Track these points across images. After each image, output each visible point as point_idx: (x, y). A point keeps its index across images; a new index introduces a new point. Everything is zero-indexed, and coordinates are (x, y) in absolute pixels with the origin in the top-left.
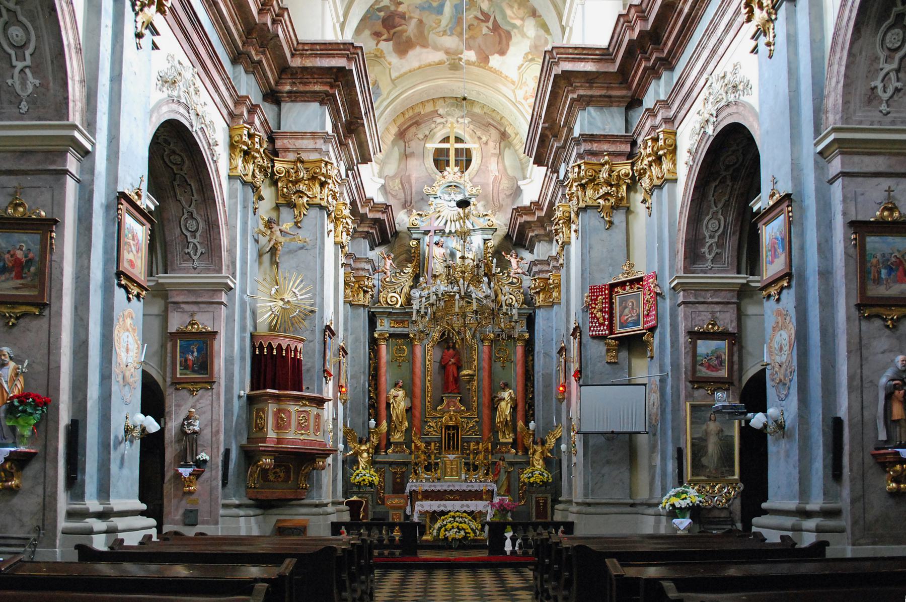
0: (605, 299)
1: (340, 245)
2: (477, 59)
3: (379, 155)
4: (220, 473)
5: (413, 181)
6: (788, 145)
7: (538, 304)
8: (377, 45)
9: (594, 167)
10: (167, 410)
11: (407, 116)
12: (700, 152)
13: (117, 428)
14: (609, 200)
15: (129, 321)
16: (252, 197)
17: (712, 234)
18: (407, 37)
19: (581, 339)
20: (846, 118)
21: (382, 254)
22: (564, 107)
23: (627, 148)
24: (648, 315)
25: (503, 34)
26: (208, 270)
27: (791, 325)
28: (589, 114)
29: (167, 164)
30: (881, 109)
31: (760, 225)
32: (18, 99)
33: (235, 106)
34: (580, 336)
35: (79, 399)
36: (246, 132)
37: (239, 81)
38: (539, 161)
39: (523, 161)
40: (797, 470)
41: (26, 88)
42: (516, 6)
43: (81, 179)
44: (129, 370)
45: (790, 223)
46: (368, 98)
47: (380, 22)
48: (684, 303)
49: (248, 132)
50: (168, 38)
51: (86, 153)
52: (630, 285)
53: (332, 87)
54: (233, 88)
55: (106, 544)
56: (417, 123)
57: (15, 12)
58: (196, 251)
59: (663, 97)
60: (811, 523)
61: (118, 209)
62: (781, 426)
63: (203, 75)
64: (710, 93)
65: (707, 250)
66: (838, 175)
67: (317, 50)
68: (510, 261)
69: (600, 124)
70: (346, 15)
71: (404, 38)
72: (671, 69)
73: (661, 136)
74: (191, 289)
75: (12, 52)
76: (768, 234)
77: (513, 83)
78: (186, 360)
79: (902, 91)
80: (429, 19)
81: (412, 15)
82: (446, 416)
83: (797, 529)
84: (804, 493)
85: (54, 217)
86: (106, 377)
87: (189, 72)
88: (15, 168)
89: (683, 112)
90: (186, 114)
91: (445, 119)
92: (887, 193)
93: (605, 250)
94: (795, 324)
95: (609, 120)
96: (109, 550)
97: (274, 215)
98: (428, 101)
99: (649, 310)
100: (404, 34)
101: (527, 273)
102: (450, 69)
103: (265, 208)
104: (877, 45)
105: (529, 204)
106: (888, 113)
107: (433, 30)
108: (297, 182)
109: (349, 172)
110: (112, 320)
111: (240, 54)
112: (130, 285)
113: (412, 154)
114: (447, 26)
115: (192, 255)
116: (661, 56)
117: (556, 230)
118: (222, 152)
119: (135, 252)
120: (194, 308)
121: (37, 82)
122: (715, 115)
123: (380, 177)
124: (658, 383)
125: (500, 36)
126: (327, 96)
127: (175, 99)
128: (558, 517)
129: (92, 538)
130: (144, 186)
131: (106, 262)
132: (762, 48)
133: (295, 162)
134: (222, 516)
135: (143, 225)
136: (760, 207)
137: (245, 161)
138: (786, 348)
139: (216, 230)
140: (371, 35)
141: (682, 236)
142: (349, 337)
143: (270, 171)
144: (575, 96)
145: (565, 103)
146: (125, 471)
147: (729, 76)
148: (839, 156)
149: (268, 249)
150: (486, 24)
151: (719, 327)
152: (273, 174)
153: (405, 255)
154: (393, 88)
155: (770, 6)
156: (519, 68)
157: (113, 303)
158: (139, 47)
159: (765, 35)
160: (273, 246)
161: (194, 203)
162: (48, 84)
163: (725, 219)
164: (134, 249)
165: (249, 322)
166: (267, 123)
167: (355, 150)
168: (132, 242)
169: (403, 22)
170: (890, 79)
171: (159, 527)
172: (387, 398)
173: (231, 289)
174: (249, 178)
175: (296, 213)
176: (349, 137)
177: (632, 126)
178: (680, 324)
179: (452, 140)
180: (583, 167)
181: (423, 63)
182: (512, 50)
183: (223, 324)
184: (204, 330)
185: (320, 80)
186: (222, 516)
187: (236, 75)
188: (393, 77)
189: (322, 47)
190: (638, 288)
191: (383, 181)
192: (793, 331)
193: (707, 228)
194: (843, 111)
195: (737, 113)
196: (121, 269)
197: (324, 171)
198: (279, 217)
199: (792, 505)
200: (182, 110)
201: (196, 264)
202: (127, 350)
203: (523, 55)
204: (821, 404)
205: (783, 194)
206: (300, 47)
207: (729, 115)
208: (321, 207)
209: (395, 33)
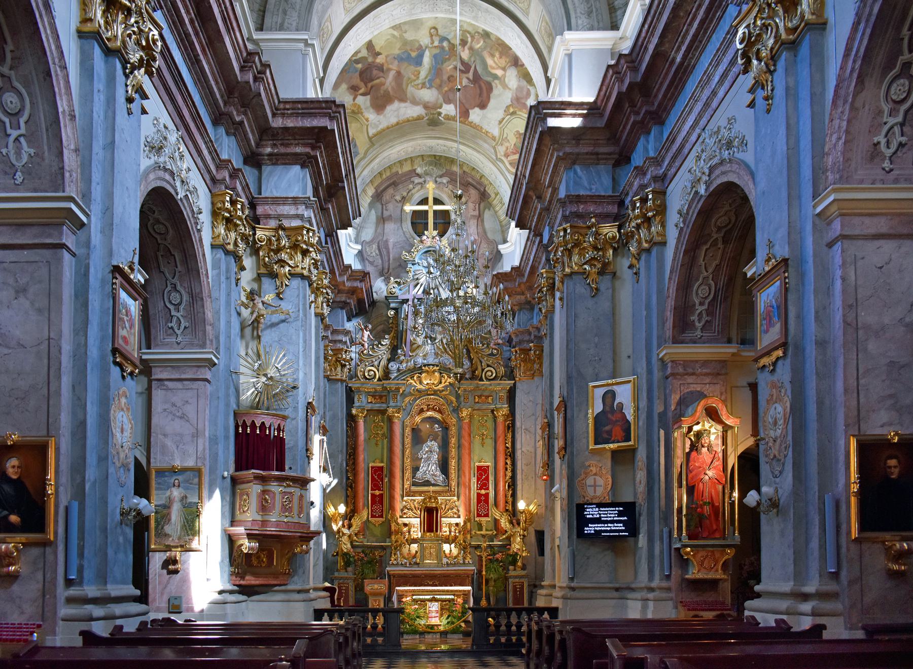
1: (320, 316)
3: (358, 220)
5: (391, 246)
8: (354, 99)
11: (384, 176)
12: (691, 213)
14: (595, 266)
15: (123, 400)
16: (235, 269)
17: (702, 300)
18: (385, 91)
22: (549, 166)
23: (613, 209)
25: (483, 85)
26: (192, 345)
27: (786, 398)
28: (575, 172)
29: (151, 235)
30: (884, 166)
31: (754, 292)
32: (11, 171)
35: (78, 481)
36: (228, 199)
37: (221, 144)
38: (521, 225)
39: (504, 223)
40: (792, 550)
41: (21, 158)
42: (497, 55)
44: (124, 451)
45: (786, 290)
46: (349, 159)
47: (357, 74)
49: (231, 198)
50: (155, 104)
53: (314, 148)
54: (216, 151)
56: (394, 184)
57: (9, 78)
58: (180, 326)
60: (807, 607)
61: (113, 284)
63: (187, 138)
65: (697, 318)
66: (837, 238)
67: (299, 109)
69: (586, 184)
71: (382, 92)
72: (662, 123)
73: (650, 197)
75: (7, 120)
76: (762, 302)
77: (494, 138)
79: (907, 146)
80: (408, 71)
81: (391, 66)
86: (103, 459)
88: (11, 242)
89: (673, 170)
90: (172, 181)
91: (423, 179)
93: (590, 319)
94: (790, 397)
96: (109, 636)
97: (255, 286)
98: (406, 160)
100: (382, 88)
101: (507, 344)
102: (429, 125)
103: (247, 277)
104: (882, 100)
105: (509, 270)
106: (891, 170)
108: (278, 250)
109: (328, 239)
111: (222, 114)
112: (124, 362)
113: (390, 218)
114: (426, 78)
115: (176, 330)
116: (651, 109)
118: (205, 218)
119: (128, 328)
121: (32, 151)
122: (707, 174)
123: (357, 242)
126: (308, 158)
128: (540, 603)
130: (136, 260)
132: (760, 102)
133: (276, 230)
135: (135, 300)
136: (755, 273)
137: (228, 229)
139: (199, 303)
140: (348, 89)
141: (670, 303)
142: (327, 413)
143: (251, 239)
145: (550, 161)
146: (121, 556)
148: (839, 219)
149: (250, 323)
150: (466, 75)
152: (254, 242)
153: (382, 326)
154: (371, 147)
155: (769, 57)
156: (500, 122)
158: (130, 112)
159: (763, 88)
162: (44, 153)
163: (716, 285)
164: (127, 325)
165: (233, 400)
166: (249, 189)
167: (335, 215)
168: (125, 318)
169: (381, 74)
170: (894, 133)
174: (231, 247)
175: (278, 284)
176: (329, 201)
177: (619, 186)
179: (431, 200)
182: (492, 103)
185: (300, 141)
187: (217, 137)
189: (305, 106)
191: (359, 247)
192: (788, 405)
193: (697, 294)
195: (731, 171)
197: (306, 238)
198: (260, 287)
199: (787, 587)
200: (167, 177)
201: (180, 339)
202: (122, 432)
205: (779, 259)
206: (282, 106)
207: (723, 173)
208: (302, 277)
209: (372, 87)
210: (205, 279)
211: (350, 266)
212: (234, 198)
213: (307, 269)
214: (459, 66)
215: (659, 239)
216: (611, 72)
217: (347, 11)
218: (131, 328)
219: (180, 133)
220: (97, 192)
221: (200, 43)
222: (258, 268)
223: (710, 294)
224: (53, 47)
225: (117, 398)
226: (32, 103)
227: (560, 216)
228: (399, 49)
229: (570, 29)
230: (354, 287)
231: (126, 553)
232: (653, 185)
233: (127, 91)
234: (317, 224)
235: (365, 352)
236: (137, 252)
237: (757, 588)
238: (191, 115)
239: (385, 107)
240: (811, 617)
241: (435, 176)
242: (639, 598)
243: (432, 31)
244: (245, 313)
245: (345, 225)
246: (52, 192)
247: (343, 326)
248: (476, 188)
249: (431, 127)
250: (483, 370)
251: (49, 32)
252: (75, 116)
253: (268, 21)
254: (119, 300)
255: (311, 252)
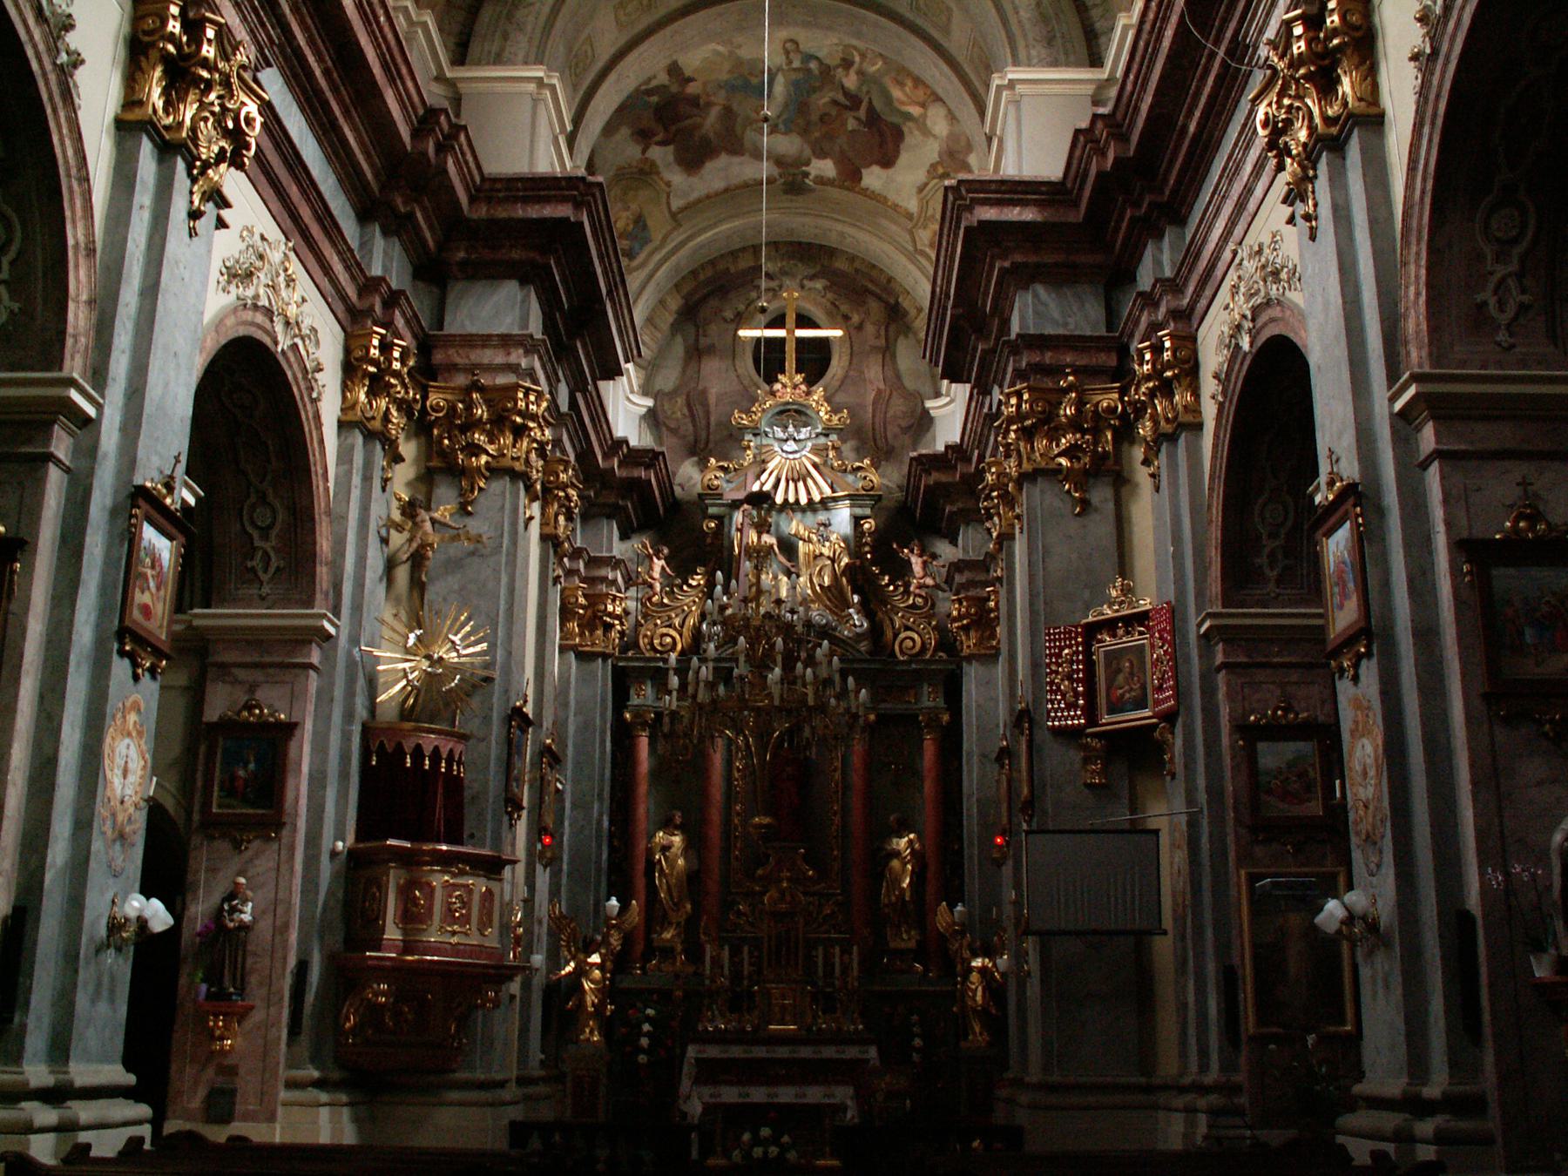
0: (1077, 653)
2: (838, 174)
4: (286, 1013)
5: (712, 400)
6: (1349, 397)
7: (966, 652)
8: (644, 151)
9: (1049, 396)
10: (190, 877)
11: (702, 277)
12: (1233, 380)
13: (95, 922)
15: (132, 718)
16: (380, 460)
19: (1031, 734)
20: (1437, 357)
21: (644, 546)
23: (1112, 360)
24: (1160, 687)
28: (1036, 296)
30: (1498, 339)
33: (360, 296)
34: (1030, 729)
36: (375, 342)
37: (371, 251)
43: (72, 466)
44: (126, 811)
46: (615, 265)
48: (1224, 665)
49: (380, 341)
51: (85, 422)
52: (1126, 626)
54: (359, 265)
55: (56, 1155)
59: (1168, 272)
60: (1426, 1127)
61: (131, 516)
62: (1372, 926)
63: (305, 251)
64: (1239, 277)
68: (909, 563)
69: (1056, 315)
70: (577, 120)
72: (1182, 222)
73: (1167, 344)
74: (256, 639)
77: (909, 216)
78: (233, 778)
80: (742, 107)
82: (773, 893)
83: (1404, 1138)
84: (1417, 1065)
85: (21, 535)
86: (83, 825)
87: (279, 249)
89: (1203, 302)
90: (268, 325)
92: (1521, 488)
93: (1074, 556)
95: (1075, 309)
98: (743, 249)
99: (1163, 678)
102: (786, 192)
103: (403, 475)
106: (1512, 346)
107: (751, 124)
109: (579, 396)
110: (103, 716)
113: (711, 350)
114: (779, 117)
115: (260, 574)
117: (987, 509)
118: (329, 382)
120: (258, 675)
121: (16, 306)
122: (1249, 317)
124: (1184, 827)
125: (881, 134)
127: (249, 302)
129: (28, 1140)
131: (103, 612)
133: (467, 390)
134: (285, 1104)
135: (171, 538)
137: (372, 393)
138: (1372, 773)
140: (633, 134)
141: (1215, 534)
143: (418, 406)
144: (1007, 264)
146: (103, 1007)
147: (1266, 251)
149: (405, 557)
150: (856, 114)
151: (1297, 714)
154: (674, 229)
155: (1303, 156)
156: (921, 190)
157: (108, 686)
158: (192, 233)
160: (417, 551)
161: (269, 477)
164: (152, 584)
166: (419, 321)
168: (149, 572)
171: (157, 1122)
172: (650, 853)
173: (329, 636)
174: (377, 425)
178: (1222, 709)
179: (791, 319)
180: (1026, 397)
181: (735, 181)
182: (904, 158)
183: (311, 708)
184: (271, 719)
186: (285, 1104)
188: (674, 208)
190: (1141, 633)
191: (650, 402)
192: (1380, 741)
194: (1430, 343)
196: (127, 623)
200: (260, 318)
201: (265, 590)
202: (125, 777)
203: (927, 167)
204: (1433, 884)
208: (515, 475)
210: (321, 483)
211: (625, 441)
212: (389, 338)
213: (522, 461)
214: (841, 98)
215: (1189, 418)
216: (1082, 138)
217: (620, 26)
218: (158, 589)
219: (291, 245)
220: (120, 365)
221: (341, 102)
222: (429, 458)
223: (1286, 518)
224: (70, 152)
225: (119, 715)
226: (25, 238)
227: (1010, 369)
228: (730, 72)
229: (1016, 63)
230: (633, 479)
231: (112, 1001)
232: (1172, 324)
233: (192, 202)
234: (548, 378)
235: (655, 599)
236: (184, 459)
237: (1357, 1089)
238: (315, 212)
239: (703, 163)
240: (1434, 1148)
241: (800, 277)
242: (1181, 1106)
243: (788, 45)
244: (397, 539)
245: (613, 372)
246: (41, 370)
247: (610, 549)
248: (879, 298)
249: (789, 197)
250: (896, 635)
251: (65, 131)
252: (94, 250)
253: (475, 49)
254: (139, 543)
255: (531, 429)
